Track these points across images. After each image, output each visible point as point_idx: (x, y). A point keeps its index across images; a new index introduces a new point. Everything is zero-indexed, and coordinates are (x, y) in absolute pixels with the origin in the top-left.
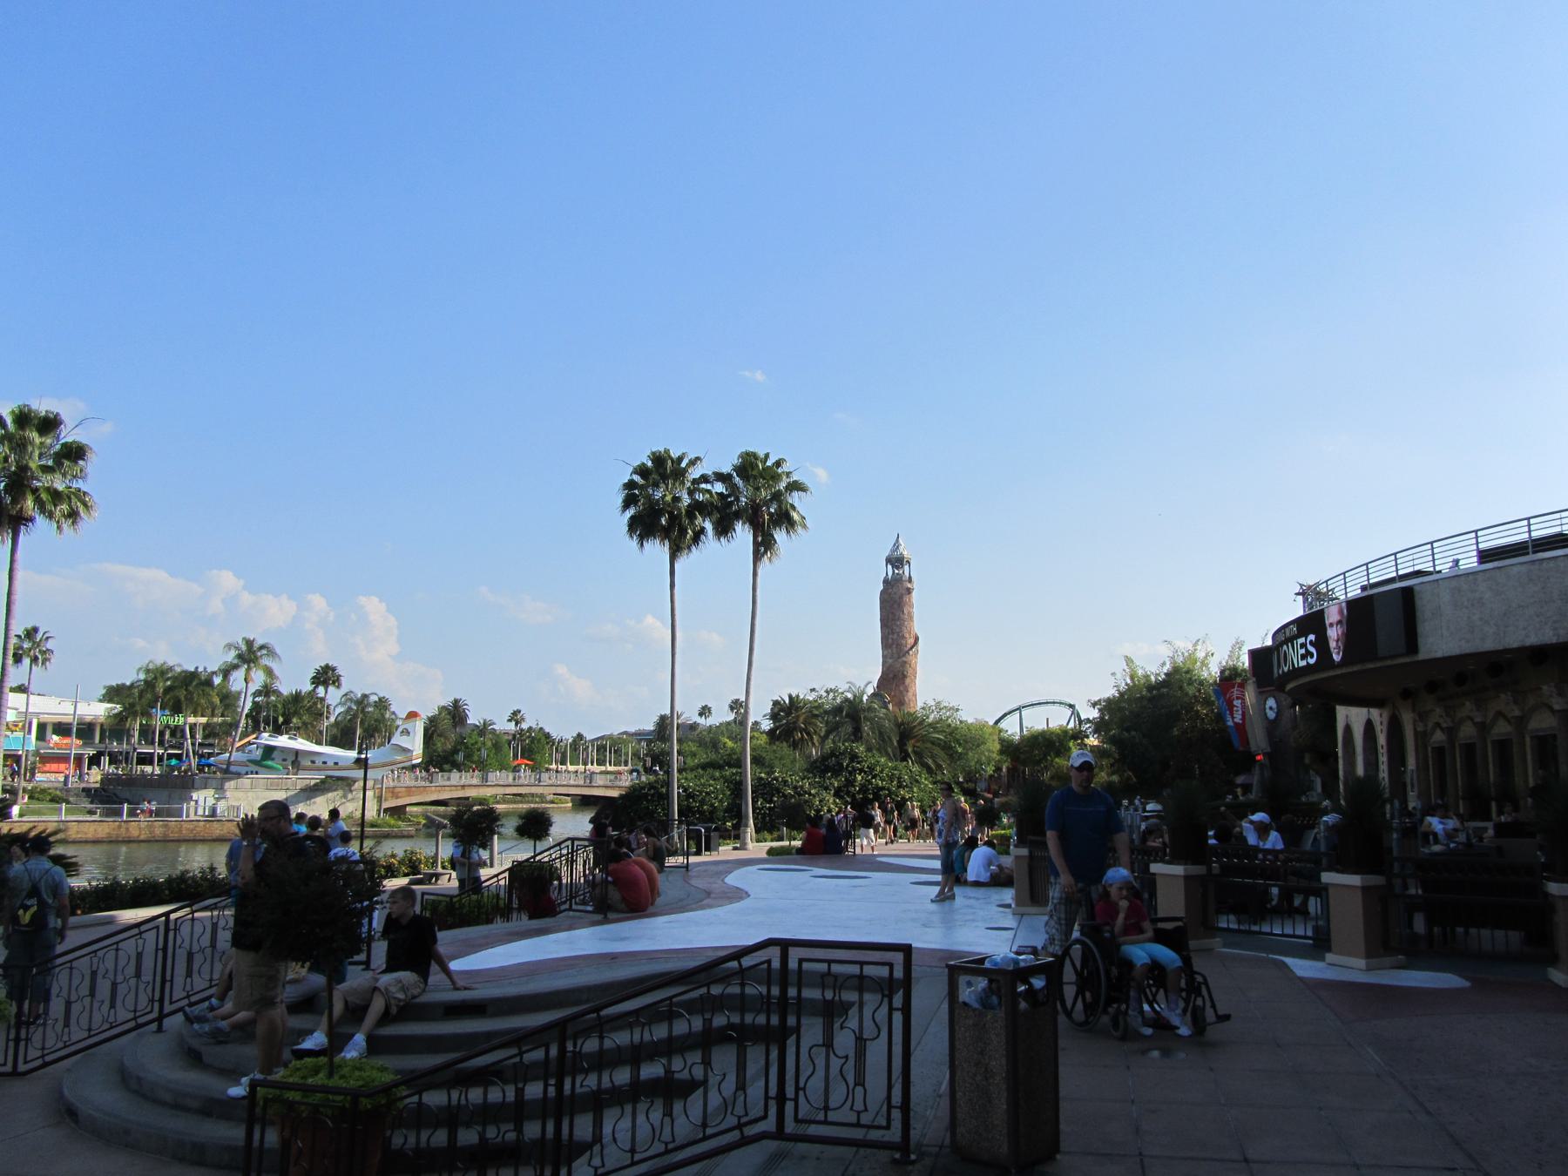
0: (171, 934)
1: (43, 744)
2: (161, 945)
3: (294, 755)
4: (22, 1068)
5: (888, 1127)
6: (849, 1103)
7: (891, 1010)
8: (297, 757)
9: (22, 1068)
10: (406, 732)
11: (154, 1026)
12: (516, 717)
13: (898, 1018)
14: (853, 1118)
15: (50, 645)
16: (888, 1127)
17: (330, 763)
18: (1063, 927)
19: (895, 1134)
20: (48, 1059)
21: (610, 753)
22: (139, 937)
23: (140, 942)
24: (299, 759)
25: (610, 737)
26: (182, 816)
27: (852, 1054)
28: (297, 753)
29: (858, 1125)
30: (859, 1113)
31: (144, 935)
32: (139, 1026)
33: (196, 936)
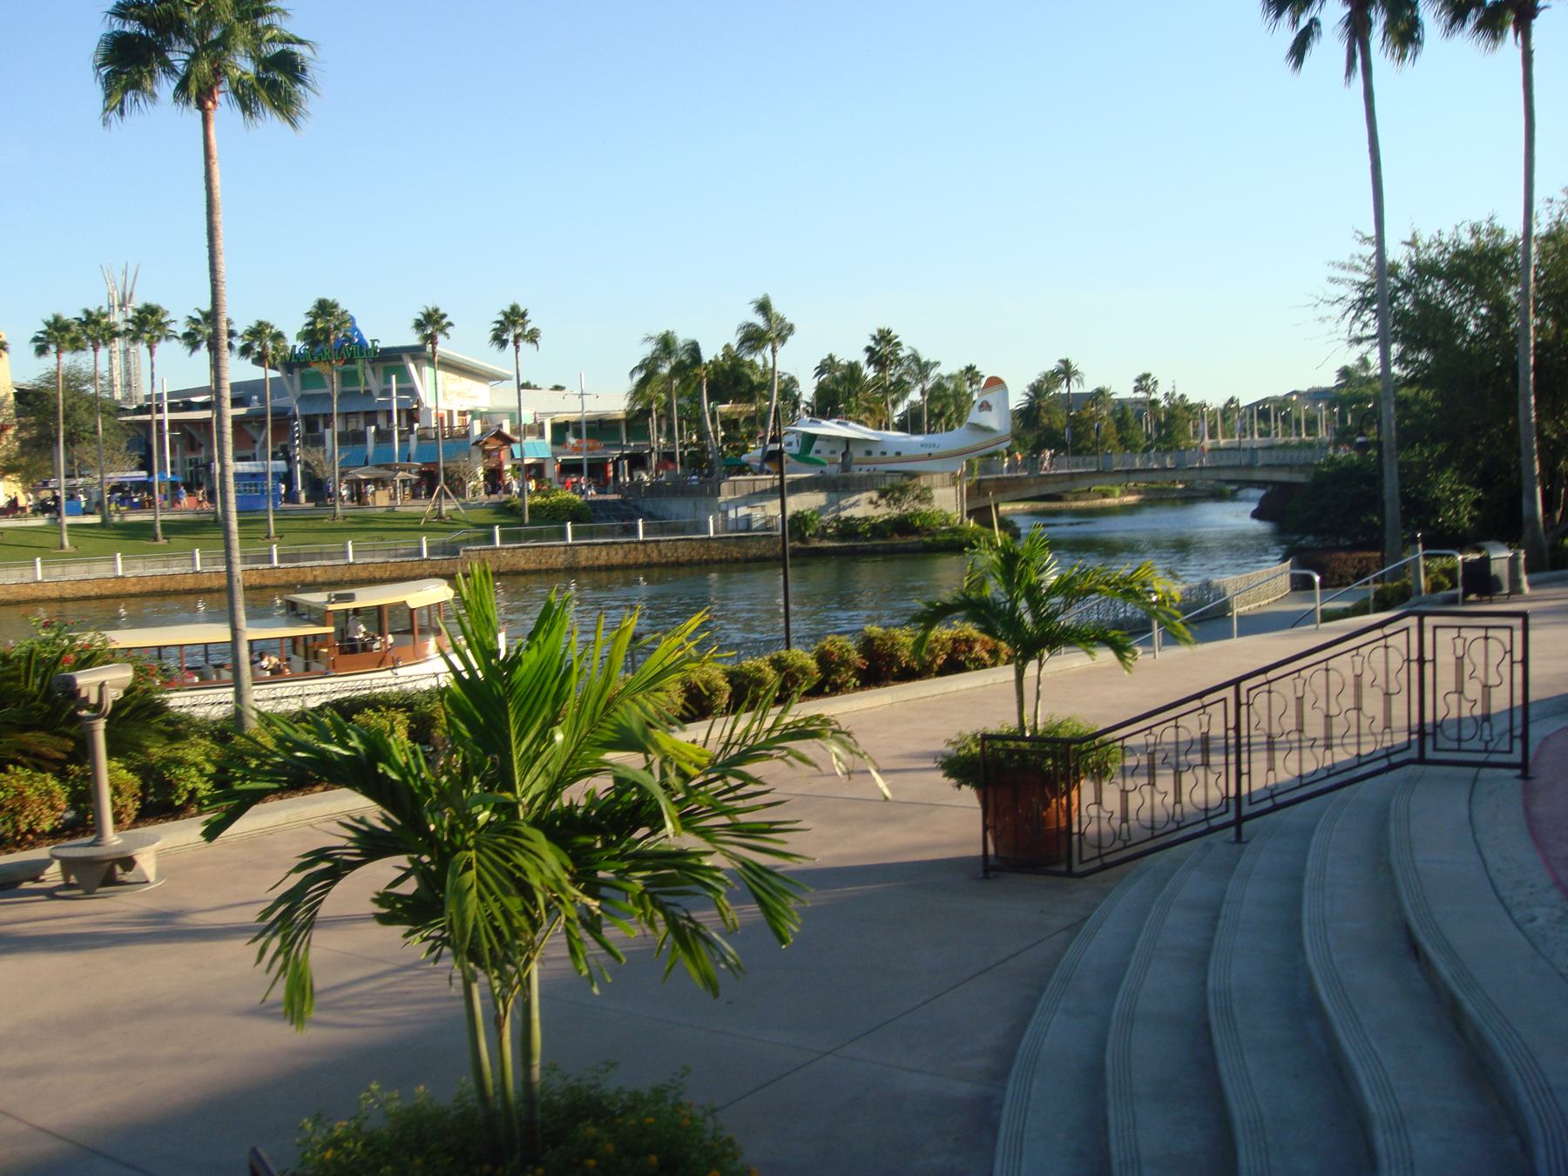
0: (1244, 709)
1: (559, 449)
2: (1231, 724)
3: (845, 445)
4: (1077, 868)
5: (1511, 751)
6: (1477, 737)
7: (1512, 663)
8: (848, 448)
9: (1077, 868)
10: (985, 406)
11: (1232, 831)
12: (1143, 382)
13: (1518, 669)
14: (1481, 746)
15: (876, 333)
16: (1511, 751)
17: (891, 454)
18: (1326, 536)
19: (1516, 757)
20: (1108, 859)
21: (1276, 420)
22: (1201, 711)
23: (1205, 718)
24: (851, 449)
25: (1274, 400)
26: (708, 532)
27: (1479, 698)
28: (848, 441)
29: (1486, 751)
30: (1487, 742)
31: (1208, 710)
32: (1211, 830)
33: (1276, 714)
